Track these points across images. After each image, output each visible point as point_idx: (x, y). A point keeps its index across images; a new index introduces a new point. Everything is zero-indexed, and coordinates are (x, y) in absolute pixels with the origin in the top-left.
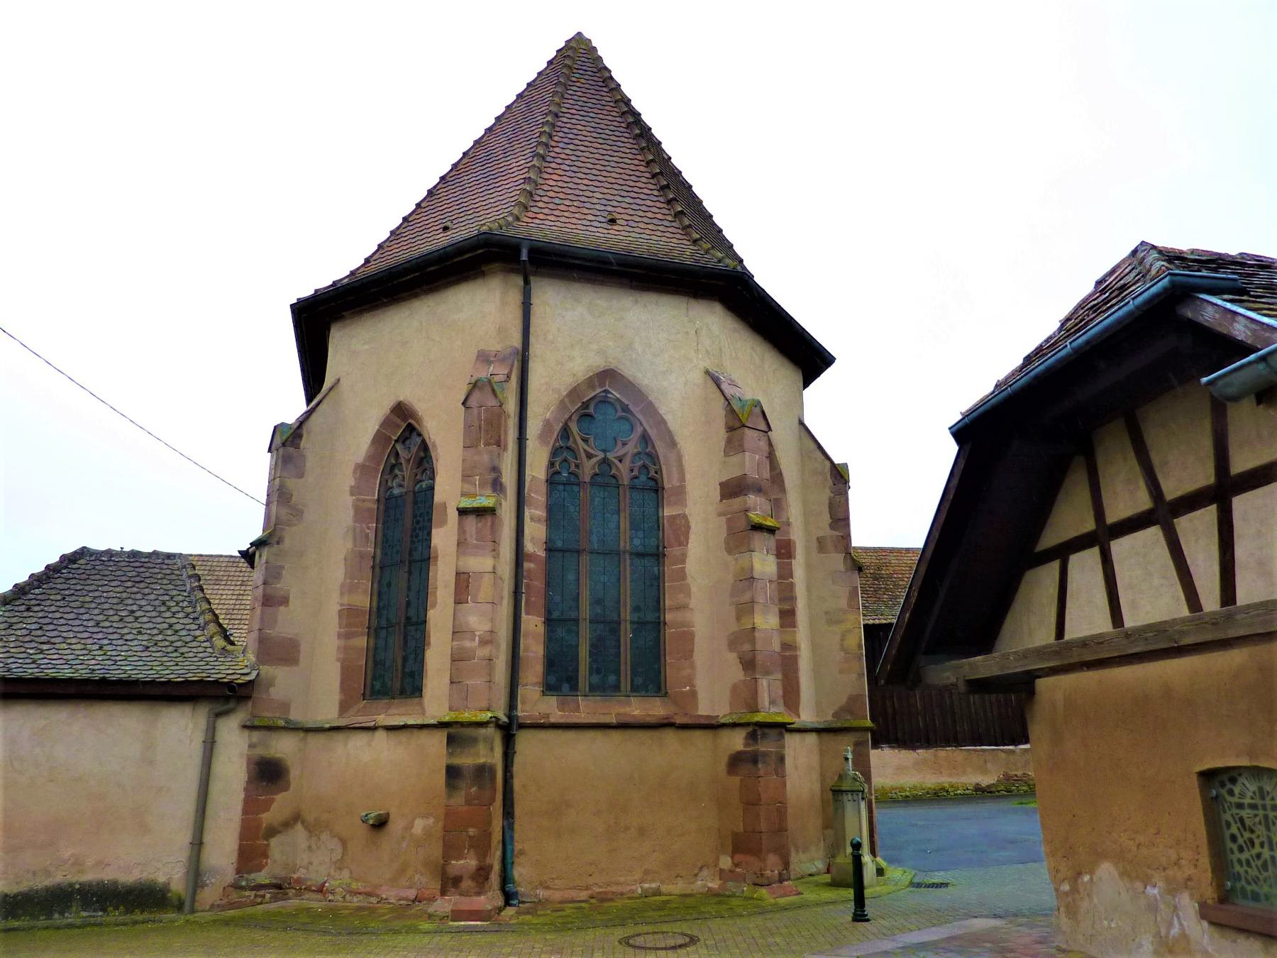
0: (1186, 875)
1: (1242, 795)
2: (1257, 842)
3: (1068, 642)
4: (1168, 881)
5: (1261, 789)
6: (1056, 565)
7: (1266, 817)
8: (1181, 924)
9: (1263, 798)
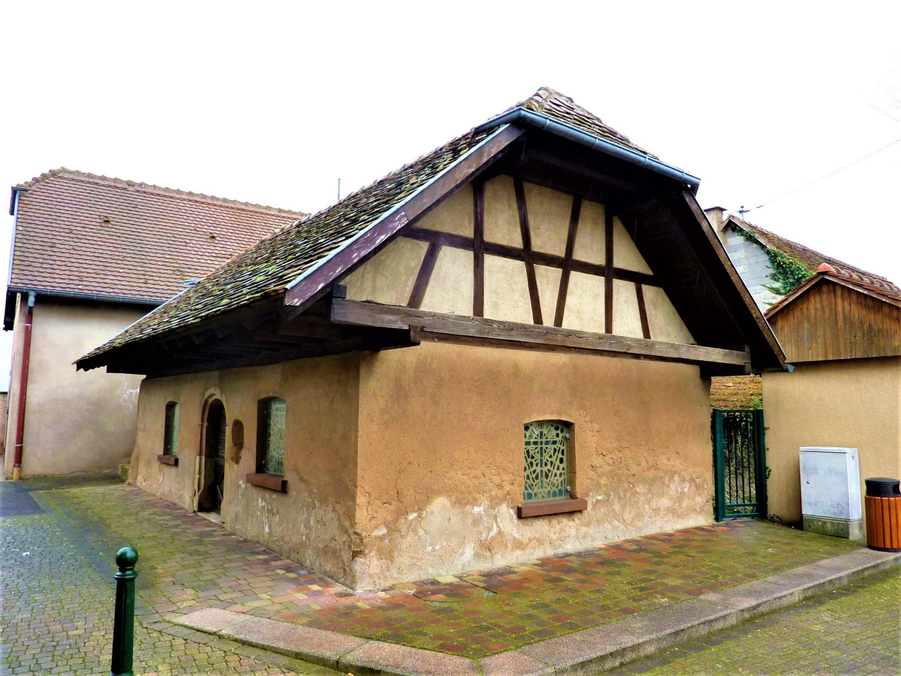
0: (505, 492)
1: (531, 437)
2: (534, 463)
3: (419, 312)
4: (492, 499)
5: (541, 433)
6: (425, 246)
7: (541, 448)
8: (498, 526)
9: (541, 438)
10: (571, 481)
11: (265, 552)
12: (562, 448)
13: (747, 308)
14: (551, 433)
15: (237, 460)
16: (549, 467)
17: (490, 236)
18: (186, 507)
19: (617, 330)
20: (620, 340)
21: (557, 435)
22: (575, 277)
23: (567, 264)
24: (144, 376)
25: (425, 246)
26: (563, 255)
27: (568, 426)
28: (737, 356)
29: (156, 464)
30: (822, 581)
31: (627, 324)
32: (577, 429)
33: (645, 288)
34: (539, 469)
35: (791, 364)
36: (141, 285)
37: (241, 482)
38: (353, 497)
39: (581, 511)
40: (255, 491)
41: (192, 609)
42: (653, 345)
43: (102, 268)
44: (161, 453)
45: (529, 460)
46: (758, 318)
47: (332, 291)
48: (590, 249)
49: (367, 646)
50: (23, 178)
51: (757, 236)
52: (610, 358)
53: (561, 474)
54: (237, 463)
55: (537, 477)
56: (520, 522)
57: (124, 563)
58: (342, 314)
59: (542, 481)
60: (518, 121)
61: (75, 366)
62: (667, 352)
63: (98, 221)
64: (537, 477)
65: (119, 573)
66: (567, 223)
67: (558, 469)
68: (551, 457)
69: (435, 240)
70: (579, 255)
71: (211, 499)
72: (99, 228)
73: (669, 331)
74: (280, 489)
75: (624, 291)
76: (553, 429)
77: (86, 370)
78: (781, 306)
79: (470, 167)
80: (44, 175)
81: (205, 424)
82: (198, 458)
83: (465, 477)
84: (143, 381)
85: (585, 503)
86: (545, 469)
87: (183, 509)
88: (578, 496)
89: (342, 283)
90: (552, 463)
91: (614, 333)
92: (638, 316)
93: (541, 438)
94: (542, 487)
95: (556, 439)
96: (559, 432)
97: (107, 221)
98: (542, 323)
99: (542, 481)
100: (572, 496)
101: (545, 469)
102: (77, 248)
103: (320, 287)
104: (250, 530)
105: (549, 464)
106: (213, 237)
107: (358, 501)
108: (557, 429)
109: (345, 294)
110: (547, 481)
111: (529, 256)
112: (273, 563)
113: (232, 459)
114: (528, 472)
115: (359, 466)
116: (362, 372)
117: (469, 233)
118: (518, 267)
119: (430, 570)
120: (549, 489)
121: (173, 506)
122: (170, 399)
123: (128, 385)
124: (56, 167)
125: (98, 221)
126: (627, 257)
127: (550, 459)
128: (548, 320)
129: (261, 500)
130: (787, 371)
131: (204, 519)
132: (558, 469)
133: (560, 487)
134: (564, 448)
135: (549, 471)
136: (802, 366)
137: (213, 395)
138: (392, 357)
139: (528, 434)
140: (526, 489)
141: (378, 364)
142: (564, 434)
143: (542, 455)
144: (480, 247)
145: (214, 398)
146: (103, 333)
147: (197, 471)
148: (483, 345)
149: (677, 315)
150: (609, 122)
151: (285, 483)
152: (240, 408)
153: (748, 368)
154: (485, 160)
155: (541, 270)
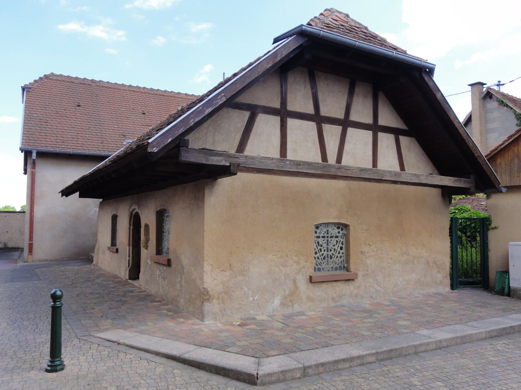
2: (323, 250)
5: (328, 231)
6: (247, 115)
7: (328, 240)
10: (348, 261)
11: (159, 301)
12: (342, 240)
13: (471, 150)
14: (334, 231)
15: (146, 247)
16: (333, 252)
17: (291, 107)
18: (122, 277)
19: (382, 165)
20: (347, 168)
21: (339, 233)
22: (351, 131)
23: (345, 123)
24: (101, 200)
25: (247, 115)
26: (343, 118)
27: (345, 226)
28: (464, 182)
29: (108, 252)
30: (504, 326)
31: (388, 161)
32: (351, 228)
33: (402, 138)
34: (325, 253)
35: (505, 187)
36: (99, 144)
37: (149, 261)
38: (202, 267)
39: (353, 280)
40: (155, 265)
41: (107, 330)
42: (378, 172)
43: (76, 134)
44: (110, 245)
45: (319, 247)
46: (479, 156)
47: (180, 143)
48: (362, 112)
49: (199, 350)
50: (29, 80)
51: (506, 101)
52: (375, 184)
53: (341, 257)
54: (147, 249)
55: (324, 258)
56: (311, 285)
57: (55, 298)
58: (188, 157)
59: (328, 261)
60: (300, 33)
61: (60, 194)
62: (411, 179)
63: (74, 105)
64: (324, 258)
65: (53, 304)
66: (346, 96)
67: (339, 253)
68: (334, 246)
69: (254, 111)
70: (354, 117)
71: (135, 272)
72: (74, 110)
73: (418, 166)
74: (166, 264)
75: (386, 141)
76: (336, 228)
77: (66, 197)
78: (500, 148)
79: (268, 63)
80: (40, 78)
81: (132, 227)
82: (128, 247)
83: (275, 257)
84: (101, 203)
85: (356, 275)
86: (330, 253)
87: (120, 278)
88: (352, 270)
89: (186, 138)
90: (335, 249)
91: (379, 168)
92: (396, 156)
93: (328, 234)
94: (328, 264)
95: (338, 235)
96: (340, 230)
97: (79, 106)
98: (327, 161)
99: (328, 261)
100: (348, 269)
101: (330, 253)
102: (60, 123)
103: (170, 140)
104: (153, 289)
105: (333, 250)
106: (144, 114)
107: (205, 269)
108: (338, 228)
109: (188, 144)
110: (332, 260)
111: (318, 119)
112: (162, 307)
113: (144, 247)
114: (318, 255)
115: (205, 248)
116: (206, 192)
117: (277, 105)
118: (312, 125)
119: (252, 312)
120: (332, 265)
121: (116, 277)
122: (114, 213)
123: (92, 204)
124: (48, 73)
125: (74, 105)
126: (388, 118)
127: (333, 247)
128: (332, 159)
129: (158, 271)
130: (501, 192)
131: (131, 284)
132: (339, 253)
133: (340, 264)
134: (344, 240)
135: (333, 254)
136: (511, 189)
137: (134, 209)
138: (224, 182)
139: (318, 231)
140: (317, 265)
141: (216, 187)
142: (343, 232)
143: (328, 244)
144: (284, 114)
145: (135, 211)
146: (75, 173)
147: (128, 255)
148: (286, 175)
149: (425, 155)
150: (373, 29)
151: (169, 261)
152: (148, 218)
153: (473, 190)
154: (279, 59)
155: (327, 128)
